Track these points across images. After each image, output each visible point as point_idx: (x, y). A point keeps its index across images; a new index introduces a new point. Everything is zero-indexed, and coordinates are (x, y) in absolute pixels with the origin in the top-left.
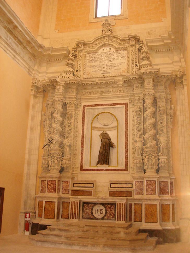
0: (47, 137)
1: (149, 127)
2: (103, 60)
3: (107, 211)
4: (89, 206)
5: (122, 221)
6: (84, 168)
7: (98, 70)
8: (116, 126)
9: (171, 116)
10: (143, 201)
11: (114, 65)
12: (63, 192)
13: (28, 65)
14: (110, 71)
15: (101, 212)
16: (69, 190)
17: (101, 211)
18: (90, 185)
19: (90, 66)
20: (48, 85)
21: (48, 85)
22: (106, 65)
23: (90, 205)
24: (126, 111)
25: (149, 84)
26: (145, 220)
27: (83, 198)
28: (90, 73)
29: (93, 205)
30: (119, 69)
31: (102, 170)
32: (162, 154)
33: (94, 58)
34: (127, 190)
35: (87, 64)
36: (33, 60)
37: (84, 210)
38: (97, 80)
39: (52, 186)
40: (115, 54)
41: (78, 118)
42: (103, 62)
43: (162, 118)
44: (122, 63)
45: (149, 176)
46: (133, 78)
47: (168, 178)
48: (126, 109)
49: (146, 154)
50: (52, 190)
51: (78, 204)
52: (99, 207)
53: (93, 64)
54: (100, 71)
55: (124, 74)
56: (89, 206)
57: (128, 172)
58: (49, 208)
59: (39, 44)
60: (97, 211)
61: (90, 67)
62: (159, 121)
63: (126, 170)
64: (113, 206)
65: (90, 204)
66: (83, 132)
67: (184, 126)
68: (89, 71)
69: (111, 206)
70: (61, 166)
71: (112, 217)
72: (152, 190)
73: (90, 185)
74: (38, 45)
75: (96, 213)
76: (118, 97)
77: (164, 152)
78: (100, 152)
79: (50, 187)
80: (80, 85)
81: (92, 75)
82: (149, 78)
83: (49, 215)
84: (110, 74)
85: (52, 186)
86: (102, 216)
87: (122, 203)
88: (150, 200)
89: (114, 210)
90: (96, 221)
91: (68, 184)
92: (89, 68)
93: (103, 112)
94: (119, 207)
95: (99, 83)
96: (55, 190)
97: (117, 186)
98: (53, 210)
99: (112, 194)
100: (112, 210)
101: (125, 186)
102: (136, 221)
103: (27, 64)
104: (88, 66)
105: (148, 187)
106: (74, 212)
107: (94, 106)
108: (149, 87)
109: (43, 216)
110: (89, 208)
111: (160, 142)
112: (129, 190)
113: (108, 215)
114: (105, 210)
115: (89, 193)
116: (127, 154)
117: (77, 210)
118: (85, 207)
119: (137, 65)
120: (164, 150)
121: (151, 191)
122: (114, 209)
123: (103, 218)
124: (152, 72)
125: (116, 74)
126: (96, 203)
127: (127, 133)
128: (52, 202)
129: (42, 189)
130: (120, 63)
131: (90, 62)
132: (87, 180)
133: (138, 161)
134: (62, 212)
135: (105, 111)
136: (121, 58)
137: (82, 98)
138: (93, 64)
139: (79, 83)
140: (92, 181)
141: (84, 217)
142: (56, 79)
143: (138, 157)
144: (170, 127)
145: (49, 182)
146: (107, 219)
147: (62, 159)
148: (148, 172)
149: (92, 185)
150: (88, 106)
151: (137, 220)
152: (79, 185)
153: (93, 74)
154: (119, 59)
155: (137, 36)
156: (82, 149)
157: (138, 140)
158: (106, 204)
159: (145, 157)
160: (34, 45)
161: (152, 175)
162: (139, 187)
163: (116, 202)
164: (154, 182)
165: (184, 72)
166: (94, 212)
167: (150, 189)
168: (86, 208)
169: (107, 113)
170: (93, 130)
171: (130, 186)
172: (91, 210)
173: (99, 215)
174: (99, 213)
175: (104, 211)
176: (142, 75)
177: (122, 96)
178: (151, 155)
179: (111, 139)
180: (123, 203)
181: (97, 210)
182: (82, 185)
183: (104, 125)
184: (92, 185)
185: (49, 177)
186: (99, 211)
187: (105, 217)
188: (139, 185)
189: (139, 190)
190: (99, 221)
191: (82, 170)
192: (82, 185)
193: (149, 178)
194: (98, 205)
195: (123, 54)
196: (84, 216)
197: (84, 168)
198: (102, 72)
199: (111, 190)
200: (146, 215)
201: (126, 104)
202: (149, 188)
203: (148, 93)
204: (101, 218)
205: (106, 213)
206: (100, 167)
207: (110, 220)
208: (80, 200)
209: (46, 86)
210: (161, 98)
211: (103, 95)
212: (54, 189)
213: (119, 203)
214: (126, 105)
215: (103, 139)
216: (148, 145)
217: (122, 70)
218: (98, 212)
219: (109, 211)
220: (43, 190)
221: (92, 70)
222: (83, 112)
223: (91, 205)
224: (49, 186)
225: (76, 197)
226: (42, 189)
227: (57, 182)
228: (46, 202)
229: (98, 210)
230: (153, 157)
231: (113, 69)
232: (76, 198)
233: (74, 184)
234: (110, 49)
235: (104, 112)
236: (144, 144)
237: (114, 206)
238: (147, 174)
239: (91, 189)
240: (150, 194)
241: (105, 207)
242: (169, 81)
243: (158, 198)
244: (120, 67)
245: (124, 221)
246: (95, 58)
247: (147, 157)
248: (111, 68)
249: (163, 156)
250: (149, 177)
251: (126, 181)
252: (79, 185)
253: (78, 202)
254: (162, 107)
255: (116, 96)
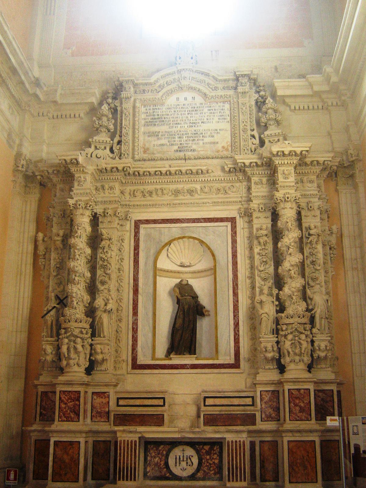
0: (53, 291)
1: (292, 272)
2: (179, 122)
3: (203, 461)
4: (160, 448)
5: (241, 480)
6: (139, 362)
7: (167, 142)
8: (211, 269)
9: (330, 249)
10: (284, 435)
11: (203, 135)
12: (94, 419)
13: (8, 124)
14: (194, 147)
15: (187, 463)
16: (108, 413)
17: (189, 460)
18: (156, 402)
19: (149, 133)
20: (55, 172)
21: (55, 172)
22: (184, 133)
23: (162, 446)
24: (232, 236)
25: (288, 178)
26: (289, 477)
27: (149, 432)
28: (148, 149)
29: (168, 447)
30: (214, 143)
31: (183, 367)
32: (319, 330)
33: (156, 117)
34: (244, 411)
35: (142, 129)
36: (16, 113)
37: (149, 458)
38: (167, 163)
39: (71, 404)
40: (206, 110)
41: (123, 249)
42: (179, 126)
43: (314, 252)
44: (220, 130)
45: (295, 380)
46: (251, 163)
47: (332, 383)
48: (232, 231)
49: (286, 329)
50: (71, 413)
51: (135, 445)
52: (183, 450)
53: (156, 129)
54: (172, 145)
55: (226, 153)
56: (160, 450)
57: (242, 372)
58: (65, 457)
59: (34, 77)
60: (178, 461)
61: (149, 136)
62: (307, 259)
63: (236, 365)
64: (215, 449)
65: (163, 444)
66: (136, 280)
67: (358, 270)
68: (147, 145)
69: (211, 449)
70: (90, 359)
71: (215, 474)
72: (302, 410)
73: (156, 402)
74: (33, 79)
75: (178, 464)
76: (215, 203)
77: (323, 325)
78: (177, 326)
79: (65, 408)
80: (129, 174)
81: (153, 154)
82: (288, 164)
83: (66, 474)
84: (196, 153)
85: (71, 404)
86: (190, 471)
87: (128, 441)
88: (299, 431)
89: (218, 458)
90: (177, 483)
91: (104, 401)
92: (147, 138)
93: (180, 236)
94: (232, 450)
95: (152, 173)
96: (78, 415)
97: (218, 401)
98: (75, 461)
99: (211, 421)
100: (215, 456)
101: (236, 401)
102: (266, 481)
103: (8, 121)
104: (144, 133)
105: (294, 404)
106: (127, 464)
107: (160, 223)
108: (288, 184)
109: (50, 478)
110: (159, 454)
111: (315, 304)
112: (249, 410)
113: (205, 469)
114: (197, 457)
115: (158, 420)
116: (238, 331)
117: (133, 459)
118: (151, 451)
119: (253, 136)
120: (323, 322)
121: (300, 412)
122: (218, 456)
123: (192, 477)
124: (295, 152)
125: (209, 153)
126: (175, 442)
127: (237, 285)
128: (71, 443)
129: (44, 412)
130: (216, 130)
131: (147, 124)
132: (148, 389)
133: (268, 346)
134: (94, 466)
135: (186, 235)
136: (218, 120)
137: (131, 203)
138: (156, 129)
139: (128, 169)
140: (162, 392)
141: (148, 474)
142: (76, 159)
143: (267, 336)
144: (330, 273)
145: (63, 396)
146: (203, 479)
147: (92, 342)
148: (290, 370)
149: (162, 400)
150: (147, 222)
151: (267, 478)
152: (132, 402)
153: (155, 152)
154: (214, 121)
155: (254, 73)
156: (135, 320)
157: (264, 301)
158: (199, 443)
159: (285, 336)
160: (23, 78)
161: (300, 377)
162: (270, 403)
163: (225, 438)
164: (306, 391)
165: (358, 154)
166: (171, 462)
167: (297, 408)
168: (153, 454)
169: (191, 240)
170: (158, 277)
171: (249, 401)
172: (164, 458)
173: (184, 470)
174: (184, 464)
175: (195, 461)
176: (273, 158)
177: (224, 202)
178: (298, 331)
179: (198, 297)
180: (242, 440)
181: (178, 457)
182: (138, 402)
183: (181, 266)
184: (162, 400)
185: (64, 384)
186: (183, 461)
187: (199, 474)
188: (270, 400)
189: (271, 411)
190: (184, 483)
191: (136, 366)
192: (138, 402)
193: (296, 384)
194: (181, 448)
195: (222, 111)
196: (147, 473)
197: (139, 362)
198: (176, 148)
199: (207, 411)
200: (290, 466)
201: (233, 220)
202: (296, 405)
203: (288, 198)
204: (188, 477)
205: (200, 464)
206: (176, 360)
207: (209, 479)
208: (140, 435)
209: (48, 173)
210: (310, 209)
211: (181, 197)
212: (75, 412)
213: (232, 442)
214: (232, 222)
215: (182, 296)
216: (290, 311)
217: (223, 145)
218: (182, 463)
219: (207, 460)
220: (45, 415)
221: (153, 143)
222: (135, 237)
223: (163, 448)
224: (63, 406)
225: (132, 428)
226: (44, 412)
227: (82, 395)
228: (56, 443)
229: (182, 459)
230: (303, 337)
231: (201, 143)
232: (131, 432)
233: (118, 399)
234: (194, 98)
235: (184, 237)
236: (281, 309)
237: (218, 447)
238: (288, 375)
239: (162, 411)
240: (298, 419)
241: (198, 452)
242: (325, 174)
243: (317, 427)
244: (216, 138)
245: (245, 480)
246: (160, 117)
247: (290, 337)
248: (196, 139)
249: (322, 335)
250: (295, 381)
251: (240, 392)
252: (132, 402)
253: (135, 441)
254: (315, 227)
255: (210, 201)
